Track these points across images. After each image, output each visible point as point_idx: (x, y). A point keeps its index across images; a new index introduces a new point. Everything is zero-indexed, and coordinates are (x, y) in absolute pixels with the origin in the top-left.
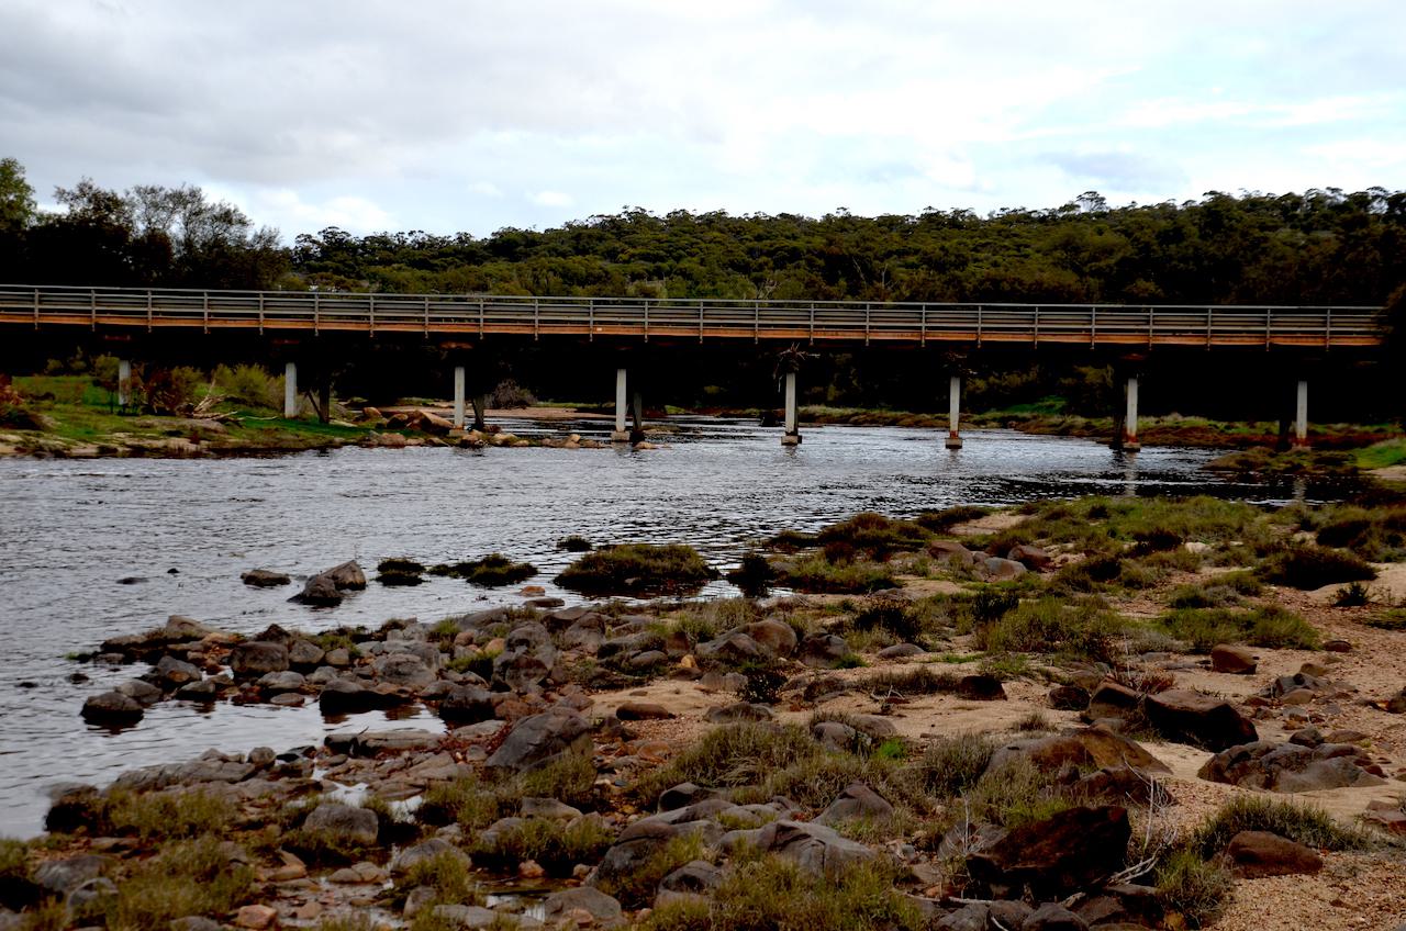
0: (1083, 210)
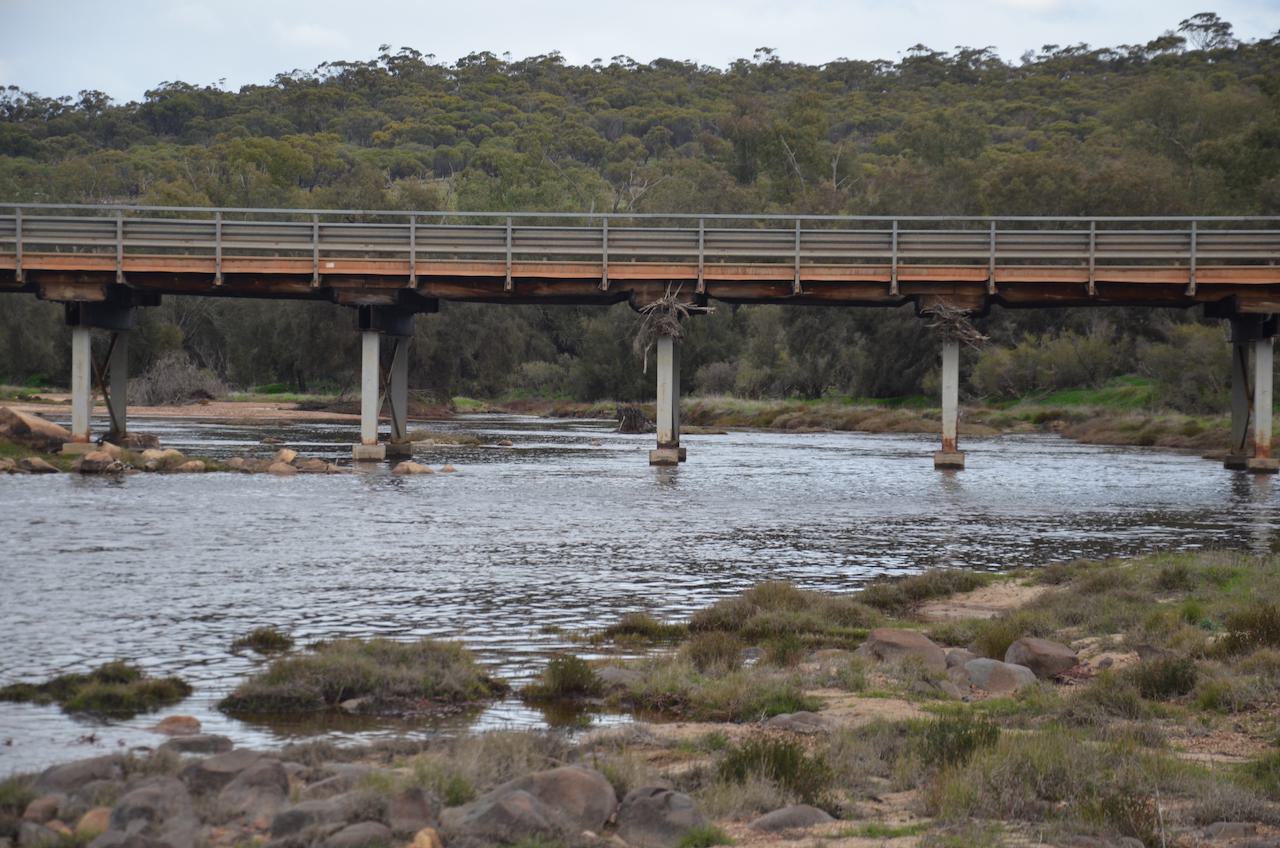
0: (1191, 46)
